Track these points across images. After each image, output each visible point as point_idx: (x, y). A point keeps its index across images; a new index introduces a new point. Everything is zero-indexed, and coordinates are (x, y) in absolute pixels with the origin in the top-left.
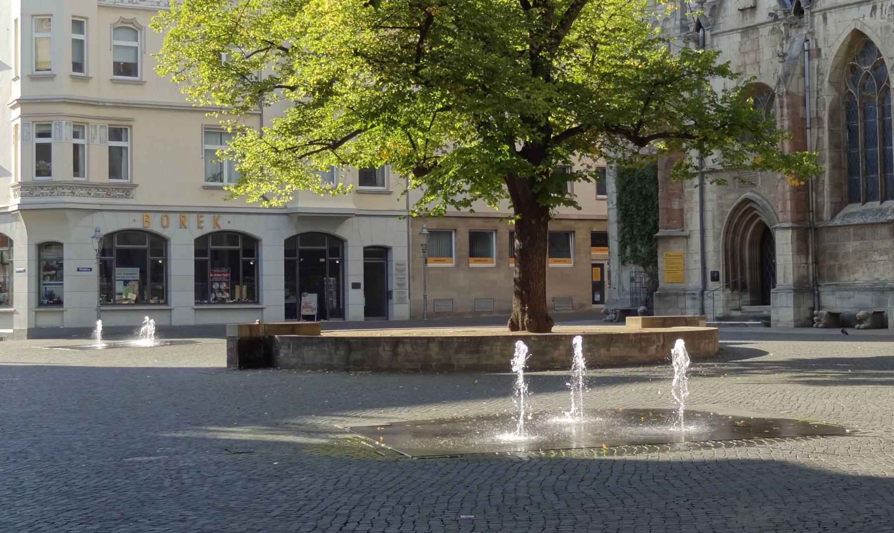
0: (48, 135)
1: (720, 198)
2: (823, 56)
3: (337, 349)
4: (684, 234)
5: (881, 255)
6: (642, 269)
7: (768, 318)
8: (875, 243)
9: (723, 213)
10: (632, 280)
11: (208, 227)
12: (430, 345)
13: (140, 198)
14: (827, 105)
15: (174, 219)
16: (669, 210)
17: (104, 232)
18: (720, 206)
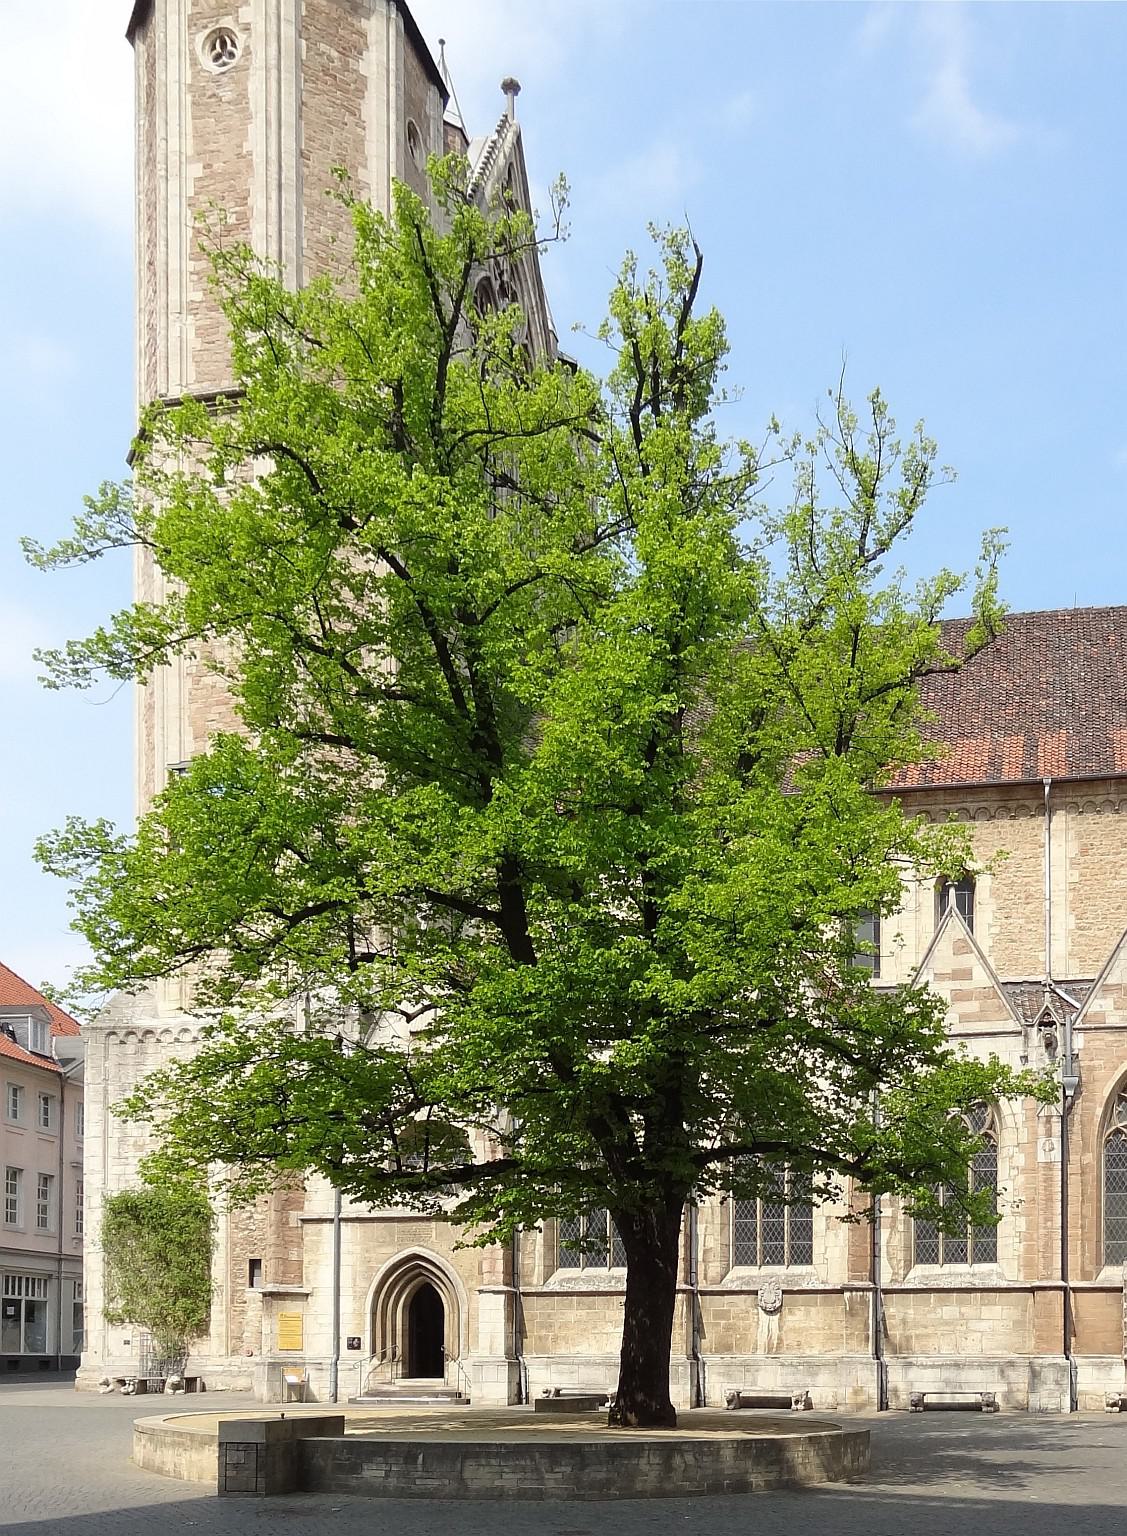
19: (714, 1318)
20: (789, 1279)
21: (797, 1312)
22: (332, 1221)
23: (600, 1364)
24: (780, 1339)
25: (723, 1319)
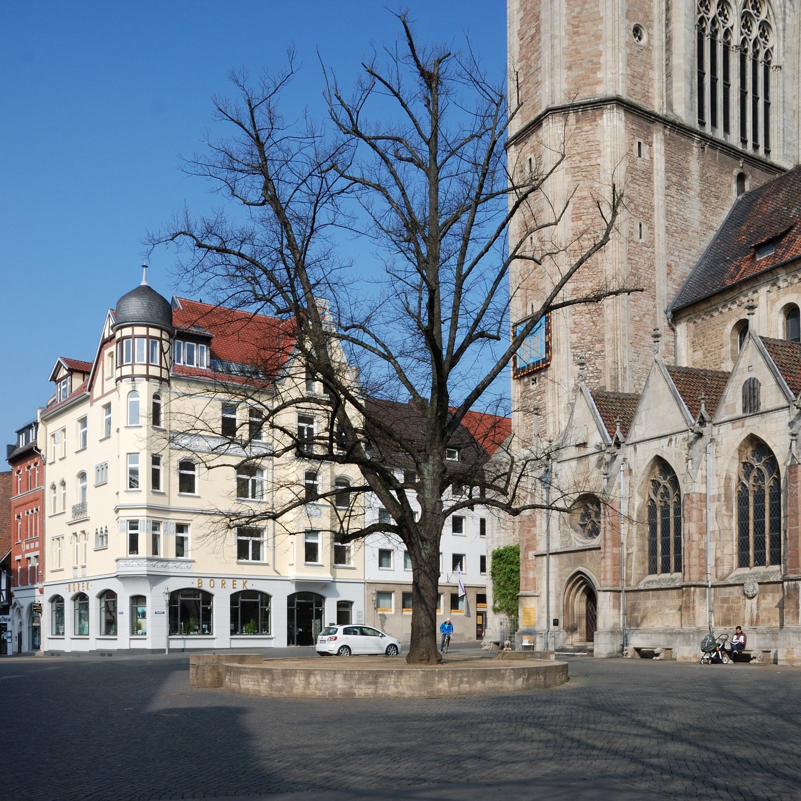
0: (136, 528)
1: (560, 570)
2: (634, 475)
3: (263, 678)
4: (536, 594)
5: (671, 610)
6: (507, 617)
7: (592, 651)
8: (667, 601)
9: (562, 580)
10: (501, 624)
11: (240, 588)
12: (336, 676)
13: (196, 569)
14: (636, 507)
15: (218, 582)
16: (526, 579)
17: (171, 590)
18: (560, 576)
19: (721, 603)
20: (765, 575)
21: (768, 598)
22: (545, 555)
23: (661, 633)
24: (758, 616)
25: (725, 603)
